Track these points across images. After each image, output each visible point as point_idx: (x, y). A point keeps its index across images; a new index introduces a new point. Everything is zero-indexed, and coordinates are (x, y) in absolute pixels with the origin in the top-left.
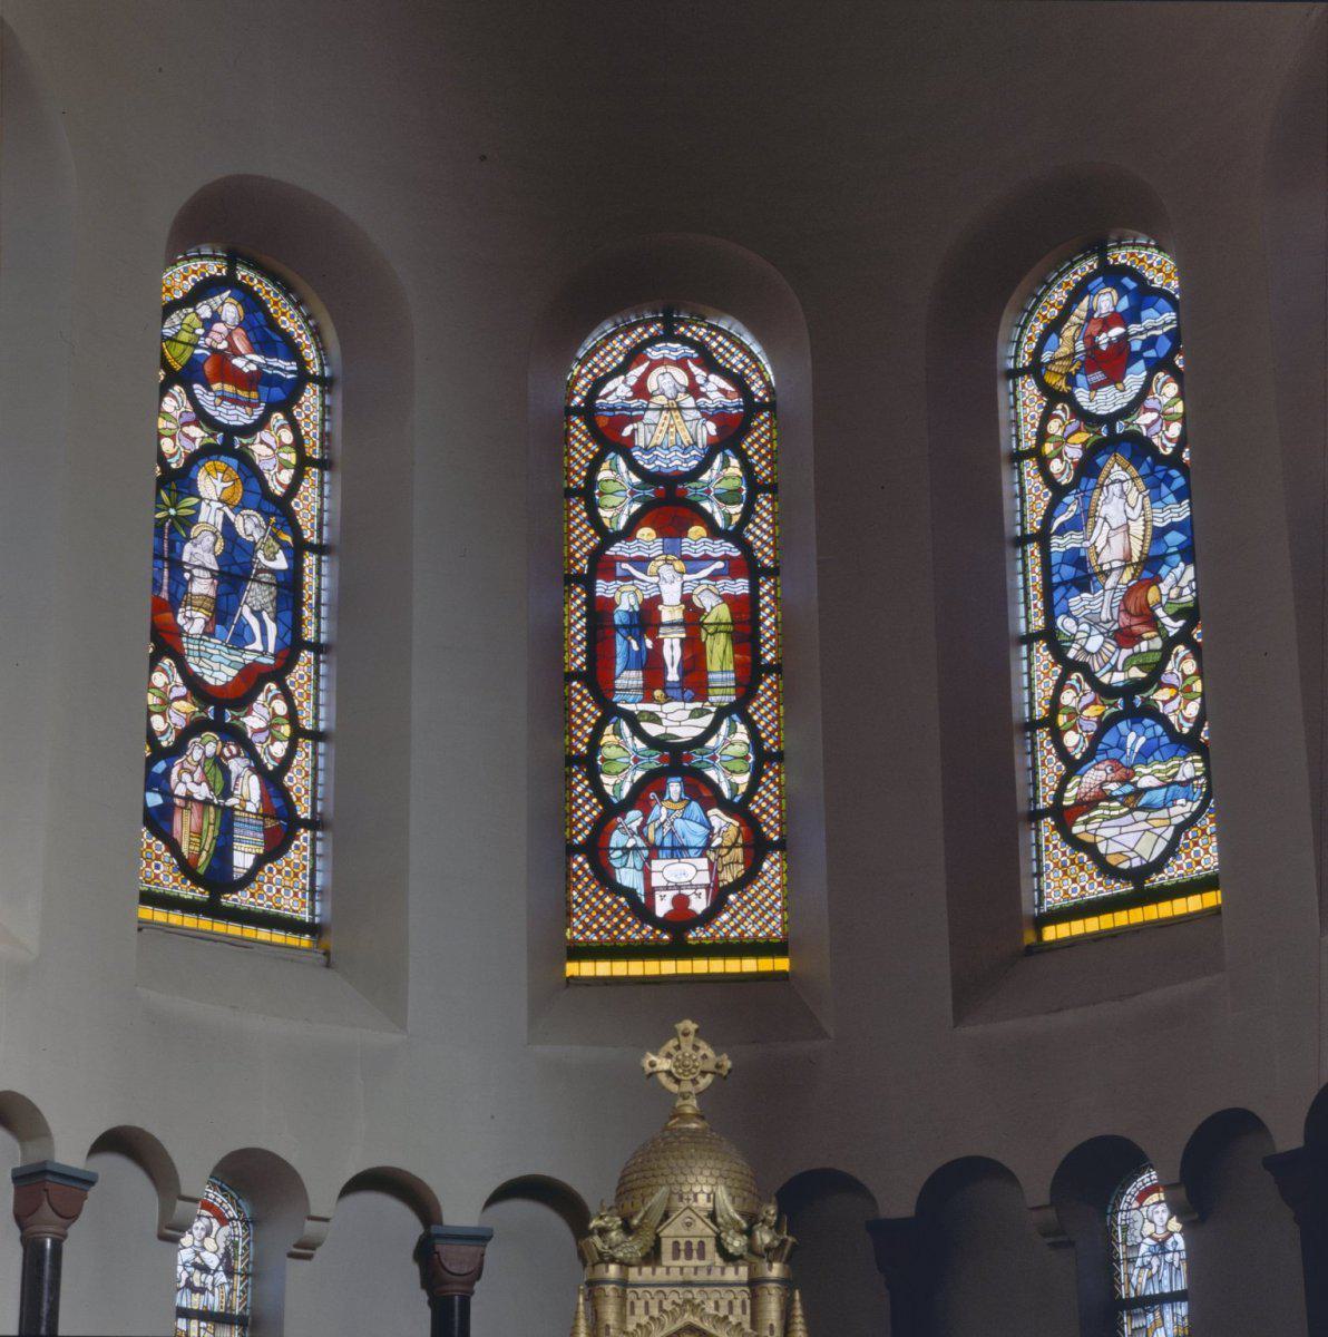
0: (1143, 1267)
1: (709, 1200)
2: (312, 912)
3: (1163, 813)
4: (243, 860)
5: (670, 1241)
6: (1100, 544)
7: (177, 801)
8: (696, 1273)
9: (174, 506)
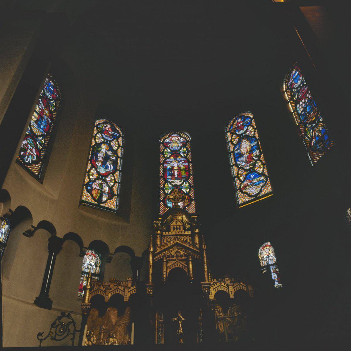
0: (265, 260)
1: (181, 218)
2: (116, 209)
3: (259, 185)
4: (104, 199)
5: (173, 227)
6: (242, 151)
7: (93, 189)
8: (178, 233)
9: (97, 148)
